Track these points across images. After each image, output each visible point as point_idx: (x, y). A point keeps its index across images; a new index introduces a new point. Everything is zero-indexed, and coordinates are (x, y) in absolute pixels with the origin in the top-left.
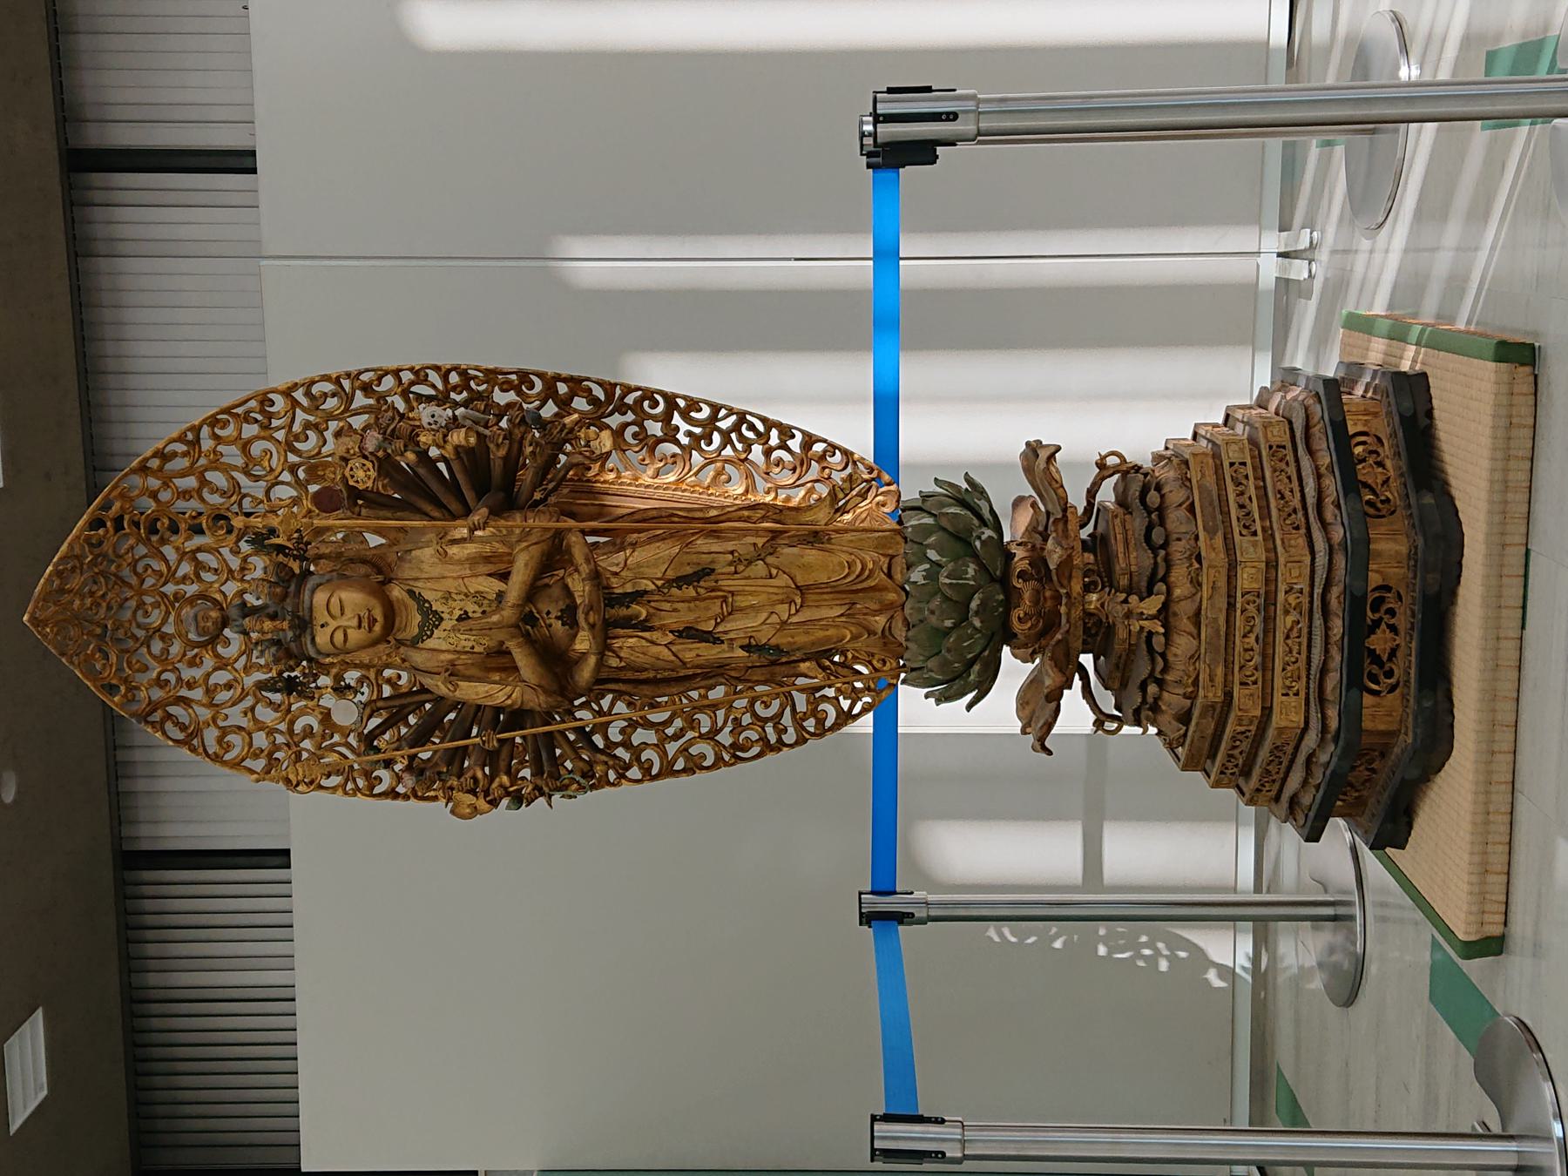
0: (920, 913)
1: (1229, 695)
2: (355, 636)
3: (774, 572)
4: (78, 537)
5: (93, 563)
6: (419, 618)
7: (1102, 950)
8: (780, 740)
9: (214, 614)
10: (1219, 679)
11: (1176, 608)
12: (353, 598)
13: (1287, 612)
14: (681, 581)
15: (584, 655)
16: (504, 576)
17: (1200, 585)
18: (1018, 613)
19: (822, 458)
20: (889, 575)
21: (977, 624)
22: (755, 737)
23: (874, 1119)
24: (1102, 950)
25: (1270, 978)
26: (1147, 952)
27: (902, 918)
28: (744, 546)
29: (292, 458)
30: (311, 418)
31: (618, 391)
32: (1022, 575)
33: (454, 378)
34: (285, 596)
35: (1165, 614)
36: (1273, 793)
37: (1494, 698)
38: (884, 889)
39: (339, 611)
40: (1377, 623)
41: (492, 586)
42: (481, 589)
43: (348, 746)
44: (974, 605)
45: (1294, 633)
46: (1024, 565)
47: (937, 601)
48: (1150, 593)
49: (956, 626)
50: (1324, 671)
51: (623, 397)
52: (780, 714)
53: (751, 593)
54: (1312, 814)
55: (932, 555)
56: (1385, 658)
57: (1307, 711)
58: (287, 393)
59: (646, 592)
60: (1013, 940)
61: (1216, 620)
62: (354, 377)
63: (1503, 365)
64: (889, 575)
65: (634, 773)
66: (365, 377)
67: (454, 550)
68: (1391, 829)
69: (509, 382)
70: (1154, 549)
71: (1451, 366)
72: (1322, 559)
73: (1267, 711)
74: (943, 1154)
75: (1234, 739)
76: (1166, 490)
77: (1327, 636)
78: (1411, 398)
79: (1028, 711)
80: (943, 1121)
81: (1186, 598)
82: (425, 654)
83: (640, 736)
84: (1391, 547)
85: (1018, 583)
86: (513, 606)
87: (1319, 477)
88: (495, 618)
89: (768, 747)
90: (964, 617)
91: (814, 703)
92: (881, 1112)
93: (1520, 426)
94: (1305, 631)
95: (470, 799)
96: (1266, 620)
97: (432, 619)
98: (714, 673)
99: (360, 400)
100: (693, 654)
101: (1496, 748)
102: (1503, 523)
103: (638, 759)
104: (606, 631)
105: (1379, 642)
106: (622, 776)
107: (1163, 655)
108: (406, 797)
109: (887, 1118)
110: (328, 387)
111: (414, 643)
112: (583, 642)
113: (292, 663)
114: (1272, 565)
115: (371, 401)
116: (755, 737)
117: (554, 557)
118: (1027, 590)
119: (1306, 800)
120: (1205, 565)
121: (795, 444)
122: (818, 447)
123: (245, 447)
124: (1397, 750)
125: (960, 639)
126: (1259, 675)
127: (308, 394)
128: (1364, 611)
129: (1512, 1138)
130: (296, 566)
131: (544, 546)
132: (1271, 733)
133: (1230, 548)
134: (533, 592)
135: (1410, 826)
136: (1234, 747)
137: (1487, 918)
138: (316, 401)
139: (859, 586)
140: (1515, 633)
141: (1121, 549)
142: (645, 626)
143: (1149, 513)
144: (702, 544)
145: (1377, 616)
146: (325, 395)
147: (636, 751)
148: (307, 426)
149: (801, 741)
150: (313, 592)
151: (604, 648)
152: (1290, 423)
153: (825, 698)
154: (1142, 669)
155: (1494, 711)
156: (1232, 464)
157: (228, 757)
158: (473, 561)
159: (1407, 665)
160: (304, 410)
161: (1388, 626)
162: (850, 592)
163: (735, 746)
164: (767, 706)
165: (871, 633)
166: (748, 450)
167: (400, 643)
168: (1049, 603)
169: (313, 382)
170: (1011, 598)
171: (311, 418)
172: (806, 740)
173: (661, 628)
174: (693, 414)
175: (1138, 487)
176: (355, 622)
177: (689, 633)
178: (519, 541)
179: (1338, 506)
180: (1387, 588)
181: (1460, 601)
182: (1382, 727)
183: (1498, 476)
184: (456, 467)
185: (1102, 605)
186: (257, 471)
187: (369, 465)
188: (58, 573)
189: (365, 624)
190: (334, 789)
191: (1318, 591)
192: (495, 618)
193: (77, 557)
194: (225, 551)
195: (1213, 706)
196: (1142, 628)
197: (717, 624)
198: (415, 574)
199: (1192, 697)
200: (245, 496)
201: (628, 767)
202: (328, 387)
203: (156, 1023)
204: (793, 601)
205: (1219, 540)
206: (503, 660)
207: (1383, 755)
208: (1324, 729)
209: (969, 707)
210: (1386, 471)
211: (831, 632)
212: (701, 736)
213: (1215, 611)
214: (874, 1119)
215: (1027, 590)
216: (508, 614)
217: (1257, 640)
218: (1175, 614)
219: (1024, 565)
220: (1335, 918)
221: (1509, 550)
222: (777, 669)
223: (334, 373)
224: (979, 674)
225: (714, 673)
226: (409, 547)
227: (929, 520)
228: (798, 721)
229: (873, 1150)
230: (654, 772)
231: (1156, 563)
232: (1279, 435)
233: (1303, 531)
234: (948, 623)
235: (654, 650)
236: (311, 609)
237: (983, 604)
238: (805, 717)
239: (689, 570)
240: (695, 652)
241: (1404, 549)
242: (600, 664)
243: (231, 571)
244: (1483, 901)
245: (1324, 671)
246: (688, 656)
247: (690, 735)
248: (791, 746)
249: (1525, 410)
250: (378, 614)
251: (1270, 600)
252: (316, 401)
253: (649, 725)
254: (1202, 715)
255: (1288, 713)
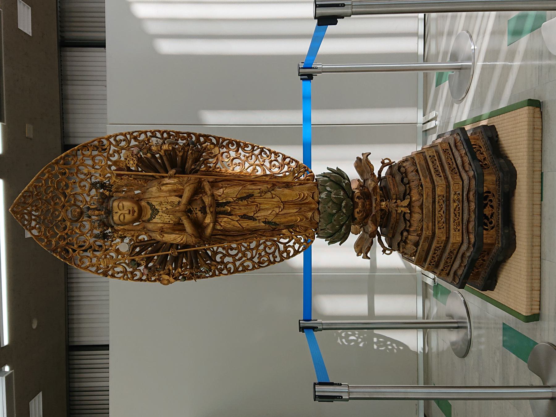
0: (320, 327)
1: (434, 233)
2: (128, 217)
3: (274, 196)
4: (32, 185)
5: (37, 195)
6: (151, 212)
7: (375, 347)
8: (274, 260)
9: (78, 210)
10: (430, 227)
11: (413, 204)
12: (127, 204)
13: (454, 201)
14: (242, 199)
15: (209, 224)
16: (181, 197)
17: (422, 195)
18: (357, 210)
19: (289, 164)
20: (313, 198)
21: (344, 211)
22: (266, 259)
23: (315, 384)
24: (375, 347)
25: (430, 355)
26: (390, 347)
27: (314, 329)
28: (264, 187)
29: (109, 163)
30: (116, 149)
31: (221, 140)
32: (358, 197)
33: (165, 135)
34: (103, 202)
35: (409, 206)
36: (447, 271)
37: (533, 226)
38: (307, 319)
39: (122, 210)
40: (486, 204)
41: (178, 199)
42: (173, 200)
43: (125, 263)
44: (343, 204)
45: (457, 209)
46: (359, 194)
47: (330, 204)
48: (404, 199)
49: (337, 212)
50: (468, 222)
51: (222, 143)
52: (275, 252)
53: (266, 204)
54: (462, 278)
55: (328, 189)
56: (489, 217)
57: (463, 237)
58: (108, 139)
59: (230, 202)
60: (346, 344)
61: (429, 206)
62: (131, 134)
63: (531, 107)
64: (313, 198)
65: (225, 272)
66: (135, 134)
67: (163, 188)
68: (489, 282)
69: (184, 137)
70: (405, 185)
71: (506, 117)
72: (466, 182)
73: (448, 238)
74: (342, 397)
75: (435, 250)
76: (406, 167)
77: (469, 210)
78: (491, 134)
79: (359, 247)
80: (341, 385)
81: (417, 201)
82: (152, 225)
83: (227, 259)
84: (490, 179)
85: (357, 200)
86: (184, 204)
87: (462, 157)
88: (177, 208)
89: (270, 263)
90: (340, 209)
91: (286, 248)
92: (317, 382)
93: (538, 129)
94: (461, 208)
95: (167, 277)
96: (446, 205)
97: (155, 212)
98: (254, 232)
99: (133, 143)
100: (247, 224)
101: (534, 245)
102: (533, 163)
103: (226, 267)
104: (217, 215)
105: (487, 211)
106: (220, 273)
107: (409, 221)
108: (145, 281)
109: (320, 384)
110: (122, 137)
111: (149, 221)
112: (208, 220)
113: (105, 228)
114: (448, 186)
115: (137, 143)
116: (266, 259)
117: (198, 190)
118: (360, 202)
119: (460, 272)
120: (424, 187)
121: (280, 159)
122: (287, 160)
123: (93, 158)
124: (494, 251)
125: (339, 217)
126: (444, 225)
127: (115, 140)
128: (482, 199)
129: (549, 387)
130: (107, 193)
131: (195, 185)
132: (450, 245)
133: (433, 182)
134: (191, 201)
135: (496, 282)
136: (435, 253)
137: (534, 307)
138: (118, 142)
139: (303, 202)
140: (539, 203)
141: (392, 187)
142: (230, 214)
143: (402, 174)
144: (249, 187)
145: (486, 202)
146: (121, 140)
147: (226, 265)
148: (115, 151)
149: (282, 260)
150: (114, 201)
151: (215, 222)
152: (449, 143)
153: (290, 246)
154: (402, 226)
155: (533, 231)
156: (430, 156)
157: (83, 266)
158: (170, 191)
159: (498, 219)
160: (114, 146)
161: (490, 206)
162: (300, 204)
163: (259, 262)
164: (270, 249)
165: (307, 219)
166: (264, 161)
167: (143, 221)
168: (368, 206)
169: (117, 135)
170: (355, 205)
171: (116, 149)
172: (283, 260)
173: (235, 215)
174: (246, 149)
175: (397, 170)
176: (127, 212)
177: (245, 217)
178: (186, 183)
179: (470, 165)
180: (489, 192)
181: (516, 194)
182: (489, 242)
183: (531, 146)
184: (165, 158)
185: (387, 206)
186: (97, 167)
187: (135, 159)
188: (23, 196)
189: (131, 212)
190: (120, 278)
191: (465, 193)
192: (177, 208)
193: (31, 192)
194: (85, 195)
195: (428, 238)
196: (402, 211)
197: (254, 214)
198: (150, 196)
199: (419, 236)
200: (92, 176)
201: (223, 270)
202: (122, 137)
203: (76, 398)
204: (280, 207)
205: (428, 179)
206: (180, 227)
207: (488, 254)
208: (469, 243)
209: (340, 244)
210: (485, 154)
211: (293, 218)
212: (248, 259)
213: (428, 204)
214: (315, 384)
215: (360, 202)
216: (182, 207)
217: (443, 212)
218: (413, 206)
219: (359, 194)
220: (458, 328)
221: (536, 173)
222: (274, 232)
223: (124, 132)
224: (345, 230)
225: (254, 232)
226: (148, 187)
227: (327, 179)
228: (281, 253)
229: (315, 396)
230: (232, 271)
231: (406, 189)
232: (446, 146)
233: (458, 174)
234: (334, 211)
235: (233, 222)
236: (112, 207)
237: (346, 204)
238: (283, 252)
239: (245, 195)
240: (247, 224)
241: (495, 179)
242: (214, 228)
243: (87, 202)
244: (532, 301)
245: (468, 222)
246: (244, 225)
247: (244, 259)
248: (278, 262)
249: (539, 123)
250: (136, 209)
251: (448, 199)
252: (118, 142)
253: (230, 255)
254: (424, 242)
255: (455, 237)
